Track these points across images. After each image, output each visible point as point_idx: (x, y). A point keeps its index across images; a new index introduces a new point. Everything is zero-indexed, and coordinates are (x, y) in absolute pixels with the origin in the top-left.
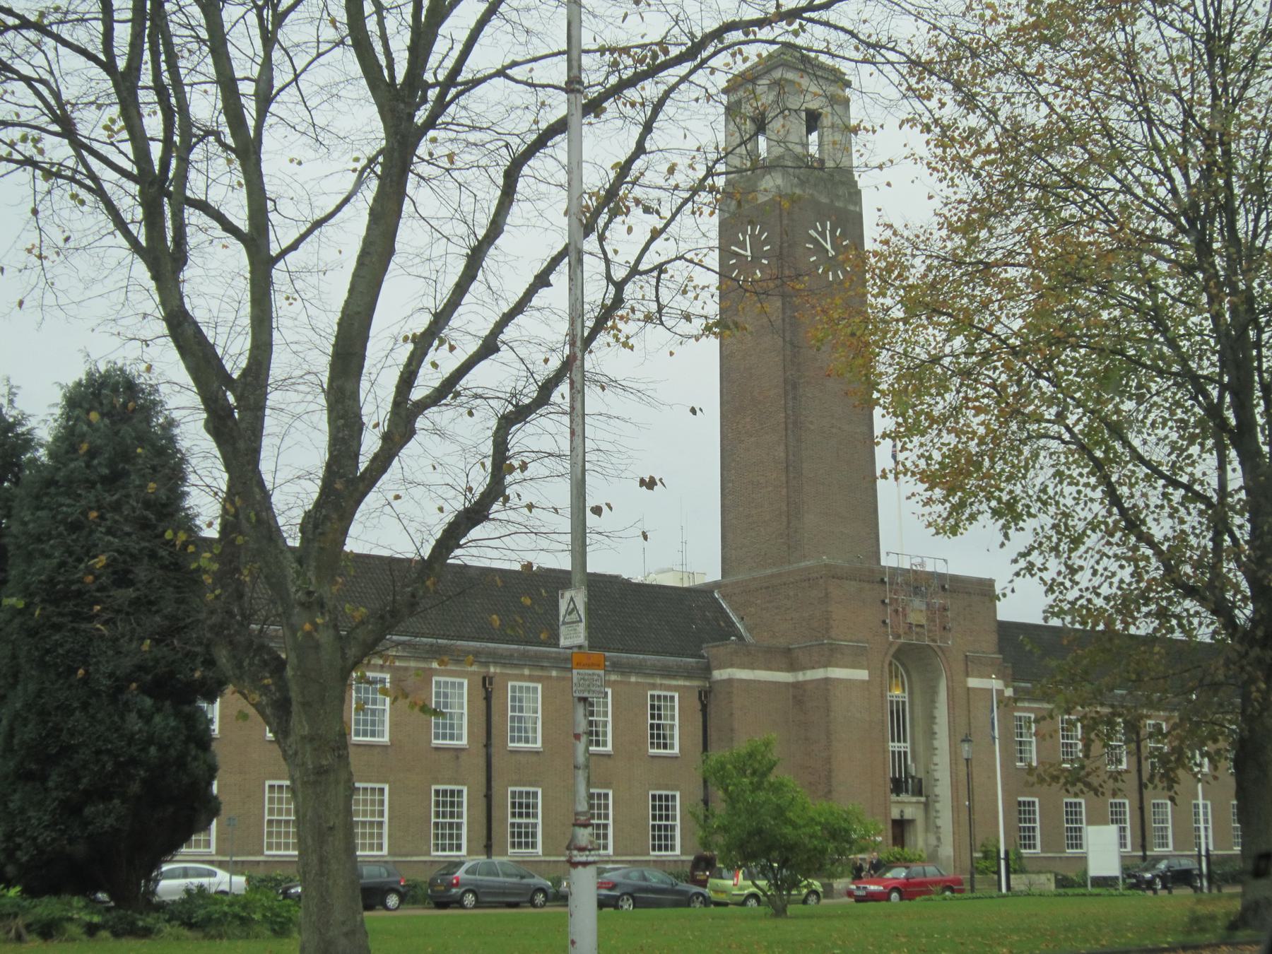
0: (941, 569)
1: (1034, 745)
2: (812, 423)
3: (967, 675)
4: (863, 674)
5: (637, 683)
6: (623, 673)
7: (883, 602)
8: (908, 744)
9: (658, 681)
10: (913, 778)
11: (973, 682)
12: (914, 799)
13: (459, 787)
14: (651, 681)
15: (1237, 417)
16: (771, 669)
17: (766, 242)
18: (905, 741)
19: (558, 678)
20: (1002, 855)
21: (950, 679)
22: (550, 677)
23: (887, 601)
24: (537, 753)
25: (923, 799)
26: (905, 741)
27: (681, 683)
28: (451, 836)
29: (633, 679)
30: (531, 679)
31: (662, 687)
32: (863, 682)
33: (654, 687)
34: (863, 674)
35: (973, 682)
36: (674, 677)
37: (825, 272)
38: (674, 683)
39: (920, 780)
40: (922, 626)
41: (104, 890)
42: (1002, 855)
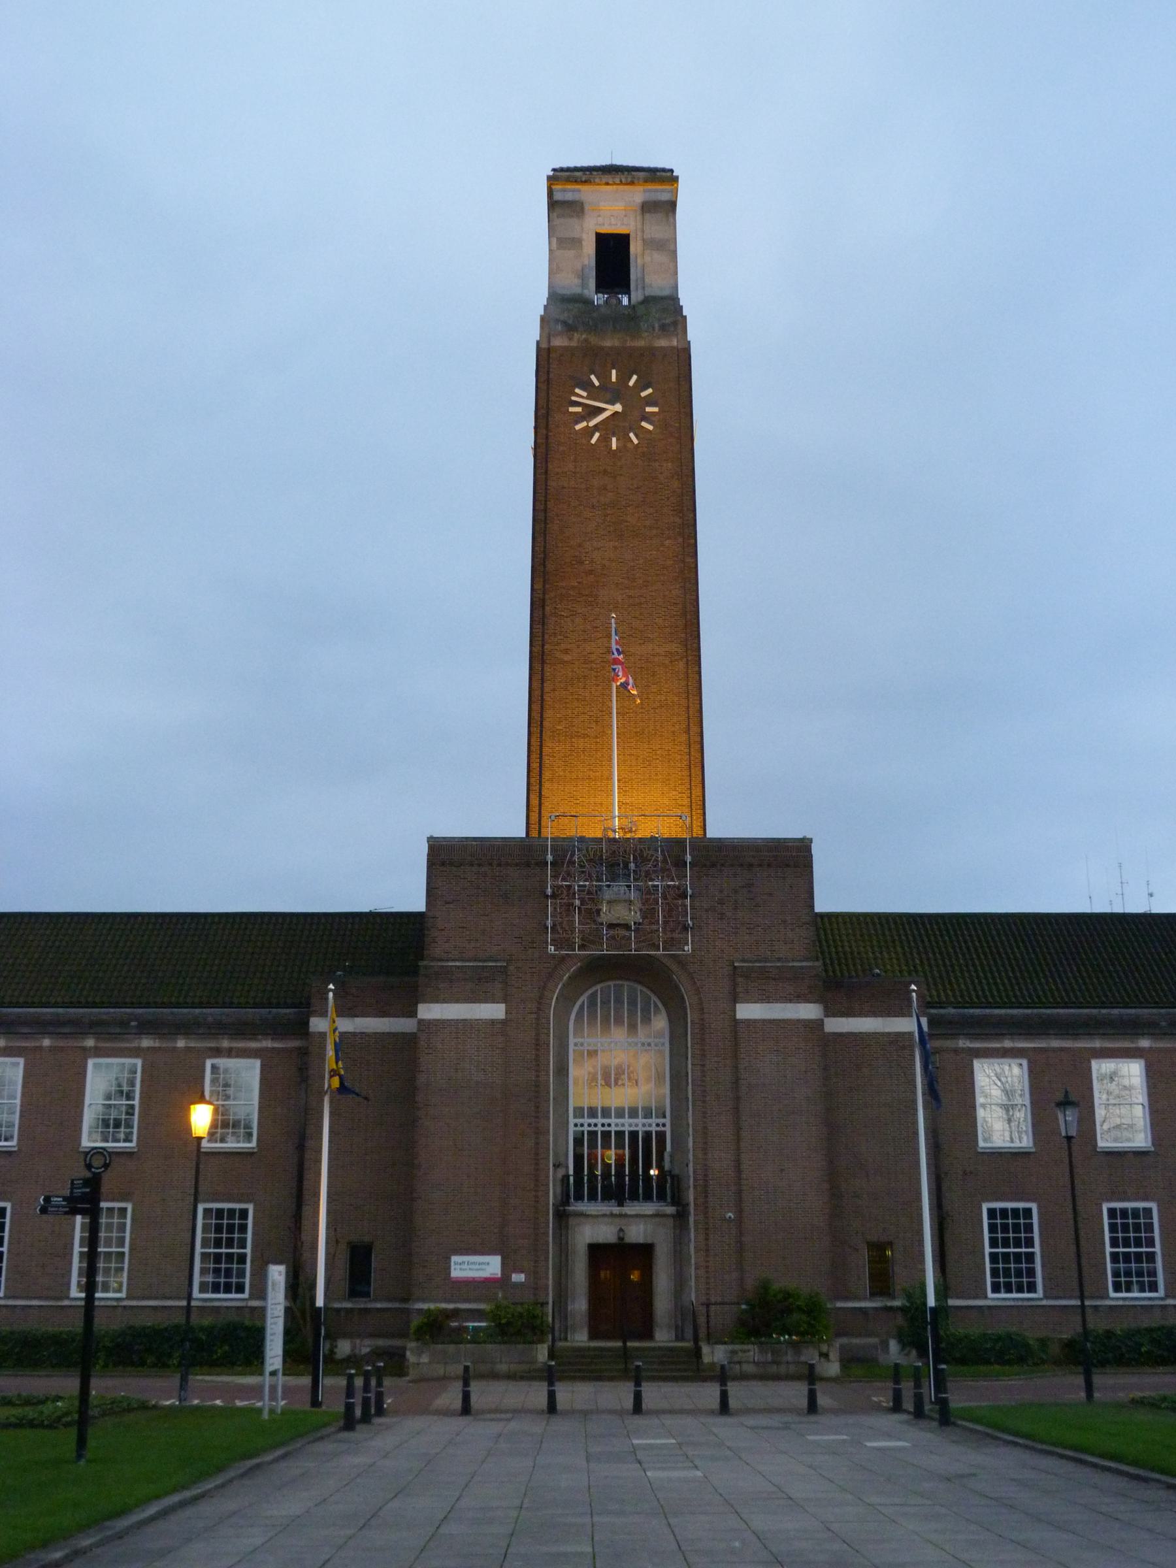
1: (89, 1117)
2: (566, 651)
4: (494, 1011)
5: (188, 1049)
6: (162, 1036)
9: (226, 1044)
11: (747, 1011)
12: (649, 1208)
14: (212, 1044)
15: (630, 378)
17: (624, 378)
19: (51, 1049)
20: (397, 1305)
22: (40, 1048)
27: (268, 1043)
28: (1005, 1228)
29: (181, 1043)
32: (493, 1022)
34: (494, 1011)
35: (747, 1011)
36: (253, 1036)
38: (254, 1045)
40: (627, 927)
41: (521, 1284)
42: (397, 1305)
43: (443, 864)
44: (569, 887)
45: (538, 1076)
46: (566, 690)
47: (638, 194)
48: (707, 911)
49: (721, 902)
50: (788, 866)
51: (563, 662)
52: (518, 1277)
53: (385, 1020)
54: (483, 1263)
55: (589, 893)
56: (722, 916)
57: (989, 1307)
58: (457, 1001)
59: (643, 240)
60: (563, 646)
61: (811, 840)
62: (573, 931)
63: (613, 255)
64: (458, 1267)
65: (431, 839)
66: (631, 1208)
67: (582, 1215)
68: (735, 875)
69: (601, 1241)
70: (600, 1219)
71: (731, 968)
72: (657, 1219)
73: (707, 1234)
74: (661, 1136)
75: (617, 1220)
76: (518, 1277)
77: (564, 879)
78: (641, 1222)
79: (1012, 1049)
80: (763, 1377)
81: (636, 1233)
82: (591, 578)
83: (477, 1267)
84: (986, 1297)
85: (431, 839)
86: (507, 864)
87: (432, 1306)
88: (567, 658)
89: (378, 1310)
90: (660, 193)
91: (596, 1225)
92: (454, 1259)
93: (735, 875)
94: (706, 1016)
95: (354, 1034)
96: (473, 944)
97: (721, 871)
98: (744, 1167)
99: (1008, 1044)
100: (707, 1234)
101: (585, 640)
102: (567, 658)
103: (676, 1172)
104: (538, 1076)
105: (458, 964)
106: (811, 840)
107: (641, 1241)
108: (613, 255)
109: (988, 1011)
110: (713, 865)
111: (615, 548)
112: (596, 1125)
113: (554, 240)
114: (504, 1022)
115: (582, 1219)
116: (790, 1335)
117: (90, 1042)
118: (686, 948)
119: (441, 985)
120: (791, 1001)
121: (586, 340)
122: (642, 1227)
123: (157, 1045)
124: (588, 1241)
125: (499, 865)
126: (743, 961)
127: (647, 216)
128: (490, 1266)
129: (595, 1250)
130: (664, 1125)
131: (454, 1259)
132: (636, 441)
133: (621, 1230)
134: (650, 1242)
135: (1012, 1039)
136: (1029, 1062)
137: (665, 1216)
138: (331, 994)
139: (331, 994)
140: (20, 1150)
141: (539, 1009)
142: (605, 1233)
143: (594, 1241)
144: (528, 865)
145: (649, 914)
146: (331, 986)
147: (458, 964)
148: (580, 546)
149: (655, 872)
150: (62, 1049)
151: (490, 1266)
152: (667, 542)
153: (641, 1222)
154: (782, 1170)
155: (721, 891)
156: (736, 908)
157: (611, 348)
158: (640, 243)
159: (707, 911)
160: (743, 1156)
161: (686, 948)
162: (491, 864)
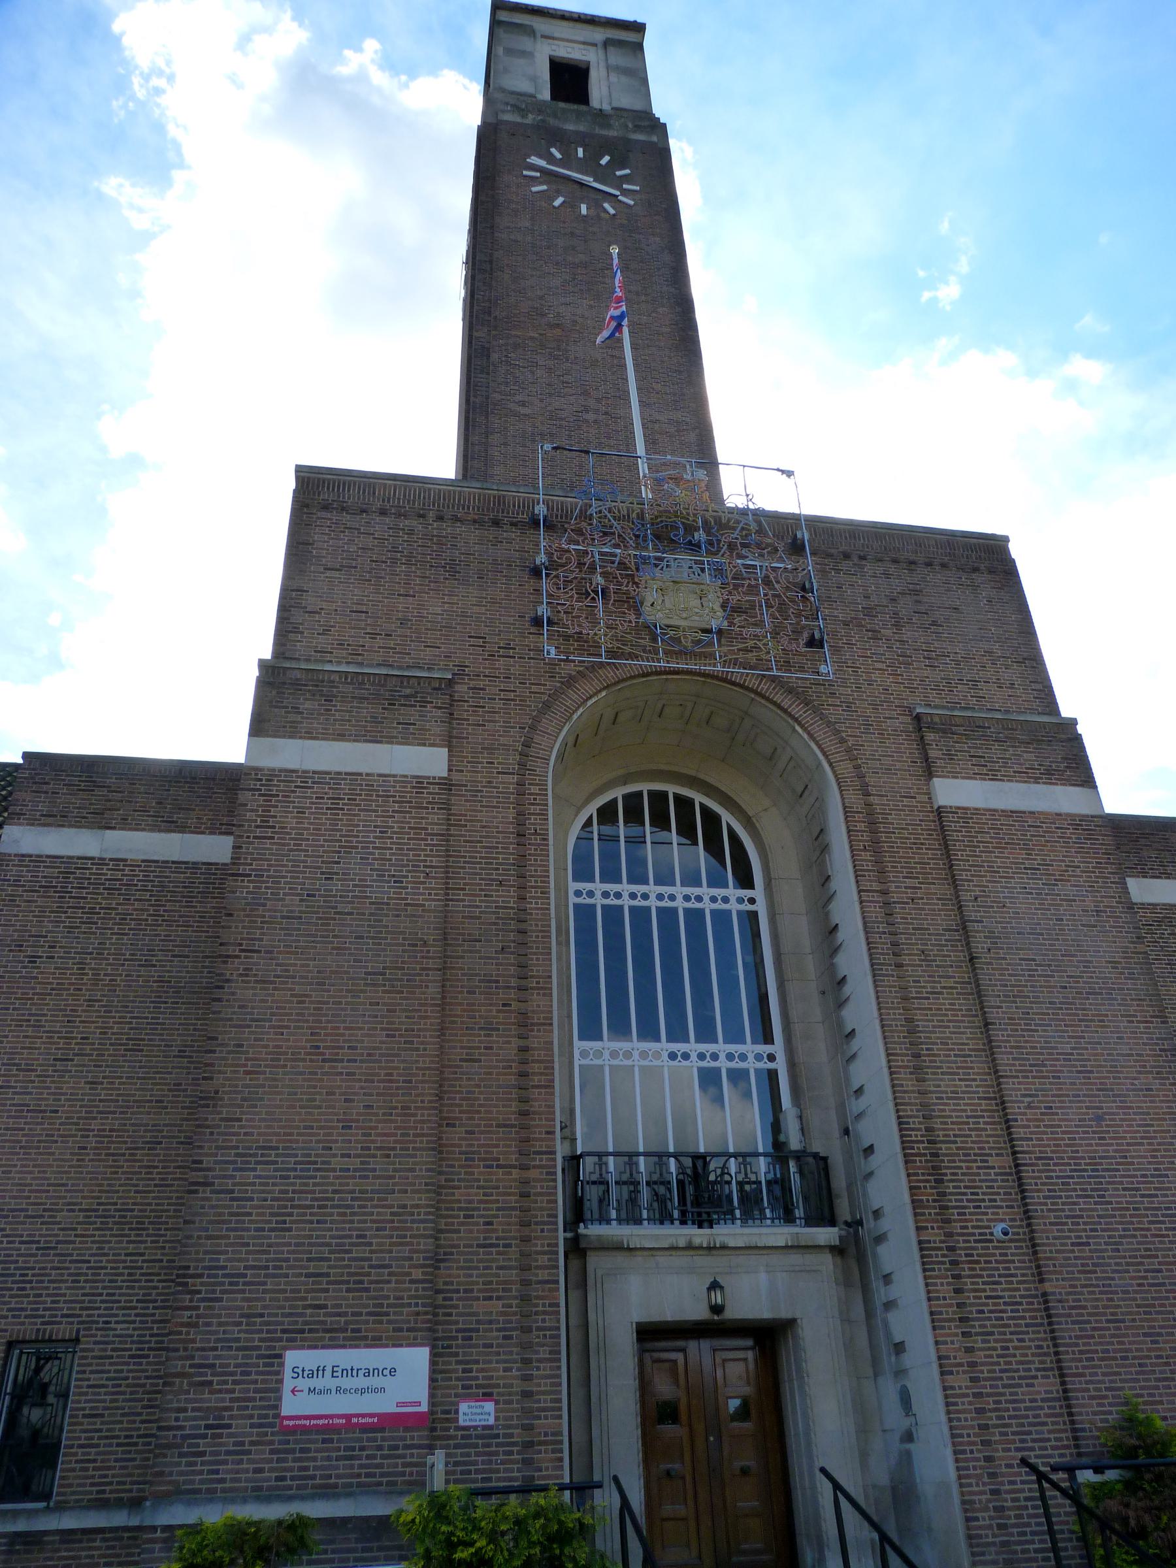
2: (523, 404)
4: (431, 761)
11: (955, 792)
12: (777, 1234)
20: (120, 1519)
25: (826, 1235)
32: (420, 783)
42: (120, 1519)
45: (522, 898)
48: (846, 624)
51: (516, 414)
52: (475, 1413)
53: (176, 837)
54: (379, 1372)
55: (622, 565)
56: (875, 635)
58: (341, 737)
60: (519, 398)
63: (569, 80)
64: (303, 1384)
65: (300, 470)
66: (729, 1233)
67: (619, 1247)
68: (887, 575)
70: (663, 1260)
72: (795, 1259)
75: (701, 1261)
76: (475, 1413)
78: (764, 1270)
81: (752, 1296)
82: (558, 332)
83: (361, 1382)
85: (300, 470)
87: (214, 1516)
88: (523, 410)
89: (67, 1535)
91: (655, 1278)
92: (293, 1358)
94: (874, 800)
95: (101, 862)
96: (379, 641)
97: (862, 567)
98: (1013, 1109)
101: (551, 395)
103: (817, 1147)
104: (522, 898)
107: (766, 1315)
111: (591, 307)
114: (446, 785)
115: (620, 1259)
116: (1102, 1546)
118: (823, 669)
119: (308, 705)
120: (1036, 781)
121: (543, 121)
122: (763, 1277)
124: (636, 1319)
125: (440, 518)
127: (611, 49)
128: (399, 1377)
129: (650, 1334)
130: (772, 1058)
131: (293, 1358)
132: (612, 211)
133: (714, 1286)
134: (784, 1314)
141: (522, 765)
142: (677, 1296)
143: (644, 1319)
144: (496, 523)
148: (541, 298)
149: (744, 545)
151: (399, 1377)
152: (660, 310)
153: (764, 1270)
154: (1099, 1119)
155: (867, 597)
157: (577, 133)
159: (846, 624)
160: (1009, 1085)
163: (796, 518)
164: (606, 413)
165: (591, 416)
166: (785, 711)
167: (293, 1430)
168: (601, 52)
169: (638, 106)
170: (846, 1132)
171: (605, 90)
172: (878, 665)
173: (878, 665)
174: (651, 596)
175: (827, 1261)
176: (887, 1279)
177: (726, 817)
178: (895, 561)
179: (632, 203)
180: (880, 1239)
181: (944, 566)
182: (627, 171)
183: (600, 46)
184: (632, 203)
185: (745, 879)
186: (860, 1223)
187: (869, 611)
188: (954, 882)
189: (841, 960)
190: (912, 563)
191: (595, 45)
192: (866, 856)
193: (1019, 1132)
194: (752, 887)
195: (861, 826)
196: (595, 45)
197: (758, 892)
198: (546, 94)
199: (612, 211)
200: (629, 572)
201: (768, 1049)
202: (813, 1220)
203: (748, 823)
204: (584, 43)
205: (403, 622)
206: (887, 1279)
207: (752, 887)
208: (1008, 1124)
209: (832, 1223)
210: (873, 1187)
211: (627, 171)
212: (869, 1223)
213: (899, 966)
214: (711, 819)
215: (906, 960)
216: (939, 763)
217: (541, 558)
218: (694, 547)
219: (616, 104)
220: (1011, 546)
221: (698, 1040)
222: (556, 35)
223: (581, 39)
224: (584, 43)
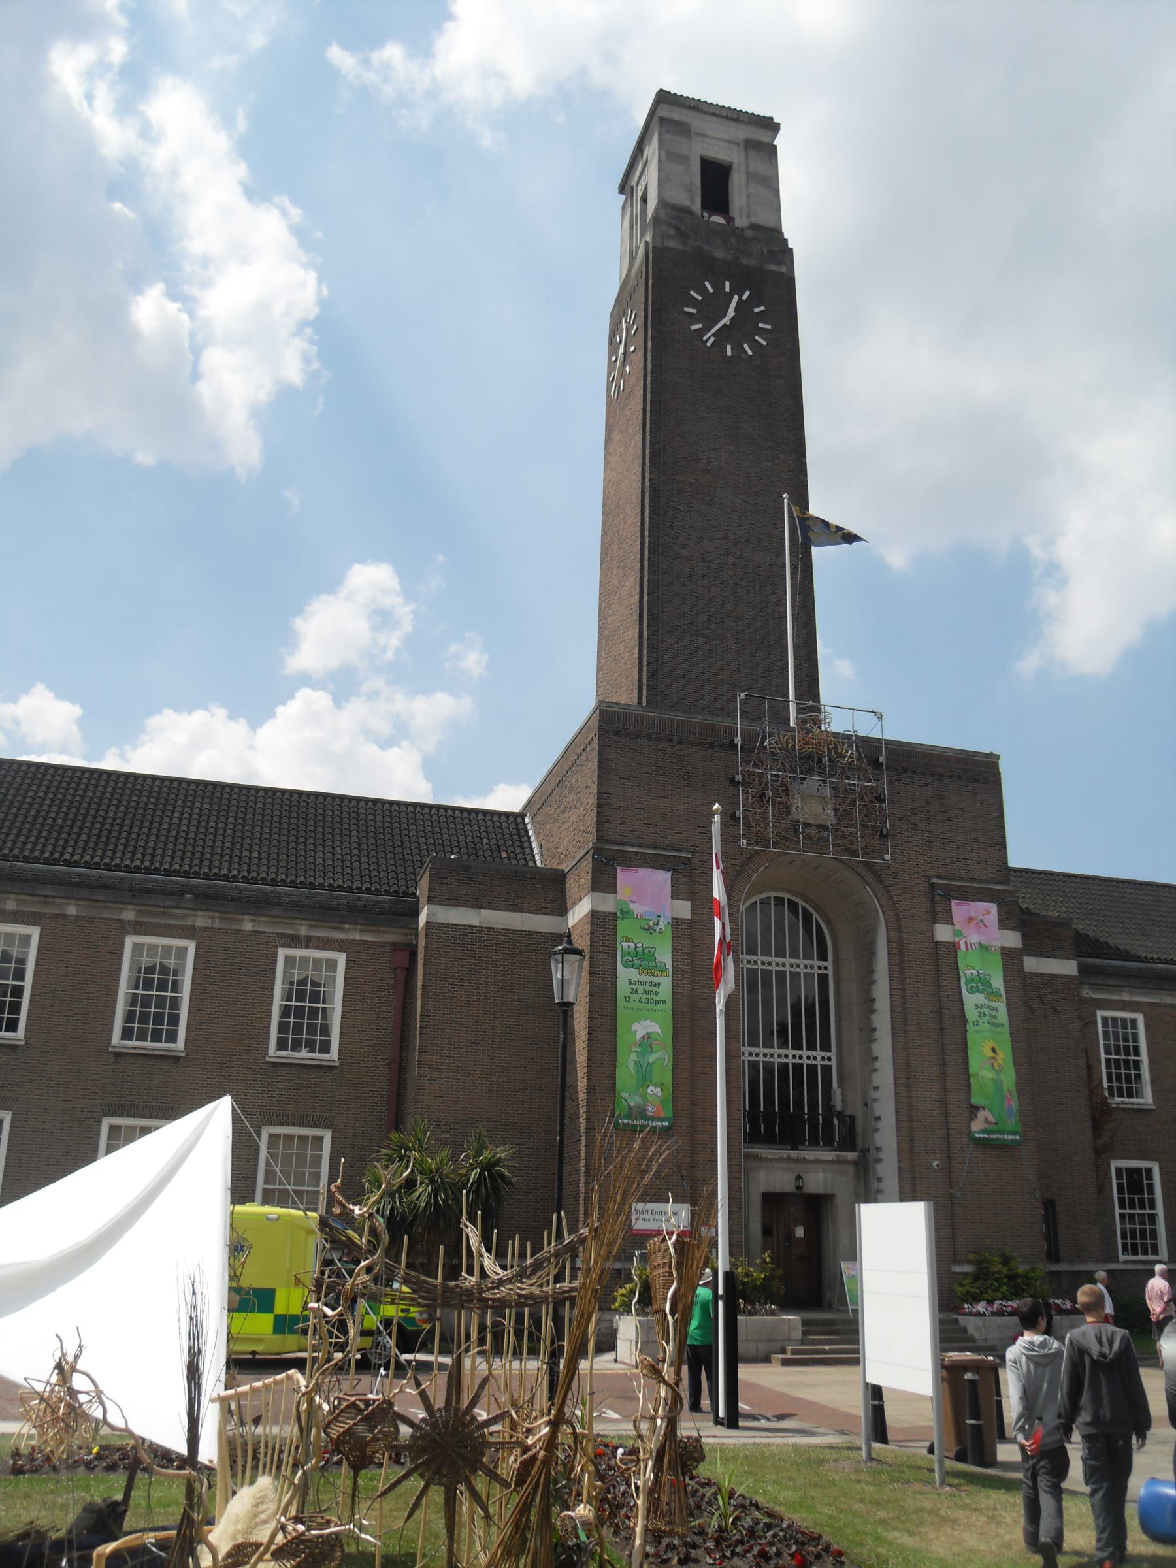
0: (867, 728)
2: (684, 546)
3: (934, 920)
7: (732, 781)
8: (832, 1054)
10: (840, 1115)
12: (829, 1156)
13: (317, 1132)
16: (522, 910)
18: (826, 1047)
21: (896, 926)
23: (739, 778)
24: (177, 1059)
25: (851, 1156)
26: (826, 1047)
30: (17, 917)
31: (308, 943)
33: (294, 941)
37: (738, 348)
39: (852, 1118)
40: (824, 827)
43: (618, 733)
44: (761, 775)
46: (685, 585)
47: (743, 133)
49: (914, 811)
50: (977, 781)
53: (519, 914)
57: (1121, 1271)
59: (748, 173)
61: (998, 757)
62: (767, 824)
63: (715, 179)
68: (927, 785)
69: (778, 1190)
70: (776, 1164)
71: (927, 884)
72: (836, 1167)
73: (914, 1185)
74: (827, 1070)
75: (793, 1165)
77: (755, 766)
79: (1130, 1002)
80: (229, 1334)
81: (816, 1182)
84: (1117, 1261)
86: (689, 743)
90: (762, 136)
93: (927, 785)
94: (904, 935)
96: (652, 829)
97: (913, 778)
99: (1126, 997)
100: (914, 1185)
102: (685, 553)
103: (849, 1112)
105: (635, 849)
106: (998, 757)
107: (821, 1191)
108: (715, 179)
109: (1107, 961)
110: (905, 771)
112: (757, 1055)
113: (664, 152)
117: (129, 915)
118: (886, 857)
122: (821, 1175)
123: (217, 925)
124: (763, 1189)
125: (680, 742)
126: (938, 877)
127: (751, 153)
132: (750, 353)
133: (799, 1177)
134: (830, 1192)
135: (1131, 994)
136: (1145, 1017)
137: (847, 1162)
138: (717, 818)
139: (717, 818)
140: (28, 1044)
144: (711, 745)
145: (843, 815)
146: (716, 806)
147: (635, 849)
150: (91, 920)
156: (928, 821)
158: (743, 176)
161: (886, 857)
162: (670, 740)
163: (879, 741)
164: (741, 557)
165: (730, 559)
166: (863, 878)
167: (637, 1235)
168: (742, 152)
169: (771, 224)
170: (866, 1105)
171: (744, 198)
172: (915, 848)
173: (915, 848)
174: (797, 803)
175: (851, 1169)
176: (880, 1180)
177: (815, 916)
178: (932, 775)
179: (765, 343)
180: (879, 1161)
181: (960, 778)
182: (762, 308)
183: (742, 147)
184: (765, 343)
185: (823, 956)
186: (868, 1150)
187: (914, 811)
188: (939, 986)
189: (874, 1017)
190: (942, 775)
191: (738, 144)
192: (896, 969)
193: (951, 1119)
194: (826, 960)
195: (895, 951)
196: (738, 144)
197: (829, 964)
198: (697, 207)
199: (750, 353)
200: (784, 789)
201: (828, 1054)
202: (842, 1147)
203: (828, 922)
204: (729, 142)
205: (663, 816)
206: (880, 1180)
207: (826, 960)
208: (947, 1115)
209: (853, 1150)
210: (877, 1136)
211: (762, 308)
212: (873, 1151)
213: (906, 1031)
214: (807, 917)
215: (910, 1028)
216: (940, 915)
217: (739, 778)
218: (822, 772)
219: (754, 220)
220: (1001, 763)
221: (793, 1048)
222: (707, 132)
223: (727, 137)
224: (729, 142)
